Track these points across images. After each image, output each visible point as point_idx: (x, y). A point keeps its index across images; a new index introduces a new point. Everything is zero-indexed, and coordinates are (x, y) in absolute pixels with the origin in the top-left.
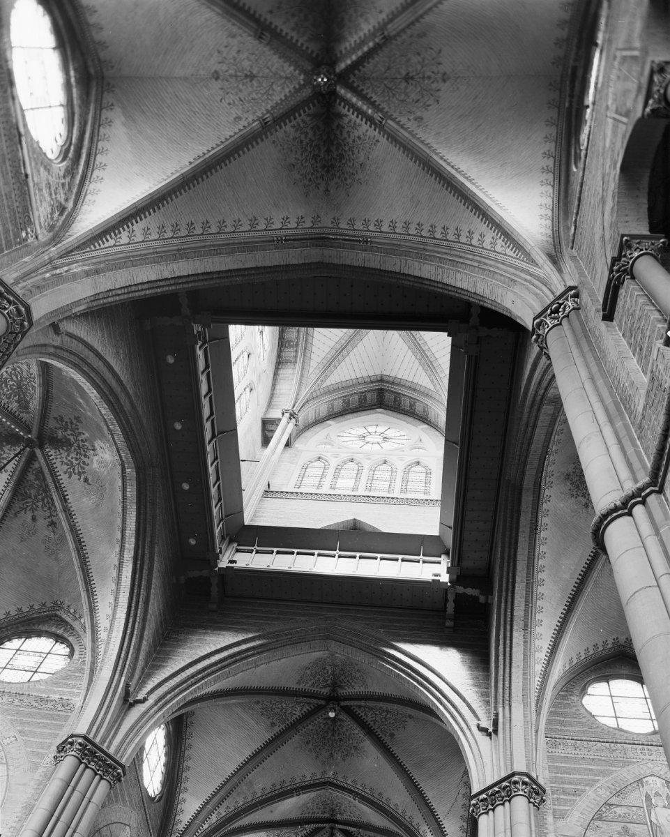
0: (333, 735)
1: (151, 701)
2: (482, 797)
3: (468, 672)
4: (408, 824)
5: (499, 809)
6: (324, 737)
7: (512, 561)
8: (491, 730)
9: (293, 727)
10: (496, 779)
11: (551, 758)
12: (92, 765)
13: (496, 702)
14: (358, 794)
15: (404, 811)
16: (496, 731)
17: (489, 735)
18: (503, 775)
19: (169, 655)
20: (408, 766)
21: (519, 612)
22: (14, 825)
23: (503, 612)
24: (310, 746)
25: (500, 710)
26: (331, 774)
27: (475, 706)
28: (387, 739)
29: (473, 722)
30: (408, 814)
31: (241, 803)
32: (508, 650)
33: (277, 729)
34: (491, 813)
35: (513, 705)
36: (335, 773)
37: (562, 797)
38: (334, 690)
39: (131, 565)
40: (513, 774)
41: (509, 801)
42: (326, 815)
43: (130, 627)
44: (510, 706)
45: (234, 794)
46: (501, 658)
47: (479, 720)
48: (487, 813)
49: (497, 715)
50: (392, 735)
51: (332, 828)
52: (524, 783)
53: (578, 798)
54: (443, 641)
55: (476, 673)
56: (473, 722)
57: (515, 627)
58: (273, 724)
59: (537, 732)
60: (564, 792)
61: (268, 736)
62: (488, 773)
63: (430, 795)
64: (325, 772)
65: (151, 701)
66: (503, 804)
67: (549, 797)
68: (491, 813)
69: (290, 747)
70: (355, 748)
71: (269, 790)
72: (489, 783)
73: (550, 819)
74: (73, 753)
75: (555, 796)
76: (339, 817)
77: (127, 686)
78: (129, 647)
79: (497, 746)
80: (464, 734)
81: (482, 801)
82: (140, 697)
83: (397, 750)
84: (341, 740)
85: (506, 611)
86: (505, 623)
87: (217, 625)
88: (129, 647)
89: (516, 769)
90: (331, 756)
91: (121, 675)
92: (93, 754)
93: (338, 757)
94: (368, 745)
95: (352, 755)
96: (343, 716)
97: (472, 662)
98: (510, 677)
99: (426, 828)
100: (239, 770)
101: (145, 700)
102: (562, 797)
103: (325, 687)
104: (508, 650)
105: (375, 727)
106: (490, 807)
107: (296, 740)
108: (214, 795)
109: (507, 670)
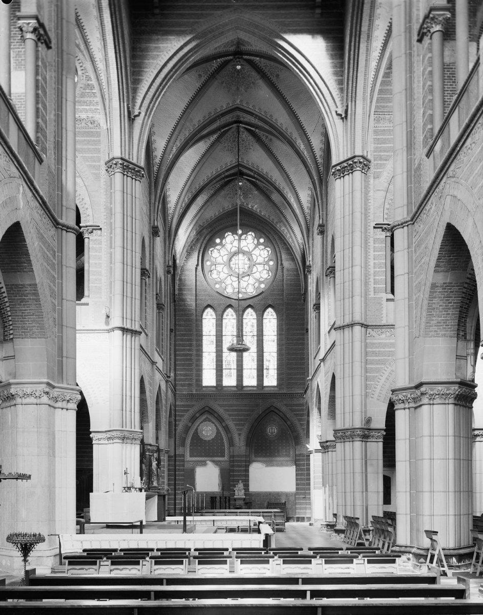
0: (238, 75)
1: (143, 114)
2: (338, 168)
3: (331, 61)
4: (289, 137)
5: (347, 177)
6: (232, 77)
7: (360, 10)
8: (343, 116)
9: (213, 76)
10: (346, 158)
11: (376, 132)
12: (130, 174)
13: (347, 100)
14: (256, 115)
15: (286, 129)
16: (346, 117)
17: (342, 118)
18: (350, 156)
19: (141, 68)
20: (288, 98)
21: (364, 28)
22: (105, 221)
23: (354, 25)
24: (224, 85)
25: (350, 103)
26: (238, 102)
27: (334, 94)
28: (274, 79)
29: (333, 108)
30: (289, 131)
31: (188, 135)
32: (356, 57)
33: (203, 79)
34: (342, 178)
35: (357, 103)
36: (241, 101)
37: (379, 162)
38: (238, 47)
39: (108, 12)
40: (354, 157)
41: (352, 173)
42: (234, 119)
43: (119, 62)
44: (355, 102)
45: (183, 130)
46: (352, 62)
47: (337, 107)
48: (340, 178)
49: (347, 106)
50: (278, 76)
51: (238, 127)
52: (360, 163)
53: (387, 162)
54: (312, 31)
55: (336, 61)
56: (333, 108)
57: (361, 40)
58: (200, 76)
59: (369, 116)
60: (381, 159)
61: (198, 85)
62: (341, 155)
63: (302, 119)
64: (234, 101)
65: (143, 114)
66: (348, 174)
67: (372, 166)
68: (342, 178)
69: (211, 91)
70: (254, 83)
71: (202, 121)
72: (342, 159)
73: (372, 180)
74: (118, 170)
75: (376, 162)
76: (242, 119)
77: (128, 108)
78: (122, 78)
79: (346, 124)
80: (328, 116)
81: (338, 170)
82: (136, 113)
83: (281, 87)
84: (243, 78)
85: (356, 27)
86: (356, 35)
87: (166, 31)
88: (122, 78)
89: (357, 154)
90: (238, 89)
91: (124, 102)
92: (127, 167)
93: (242, 89)
94: (261, 82)
95: (252, 88)
96: (248, 67)
97: (332, 55)
98: (357, 79)
99: (301, 141)
100: (184, 113)
101: (140, 113)
102: (379, 162)
103: (232, 46)
104: (356, 57)
105: (266, 71)
106: (342, 175)
107: (216, 83)
108: (172, 134)
109: (355, 74)
